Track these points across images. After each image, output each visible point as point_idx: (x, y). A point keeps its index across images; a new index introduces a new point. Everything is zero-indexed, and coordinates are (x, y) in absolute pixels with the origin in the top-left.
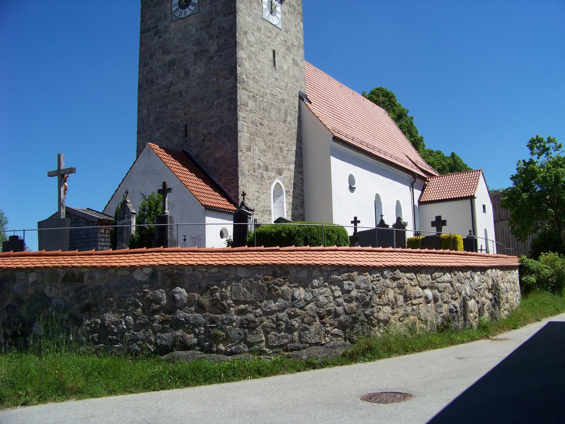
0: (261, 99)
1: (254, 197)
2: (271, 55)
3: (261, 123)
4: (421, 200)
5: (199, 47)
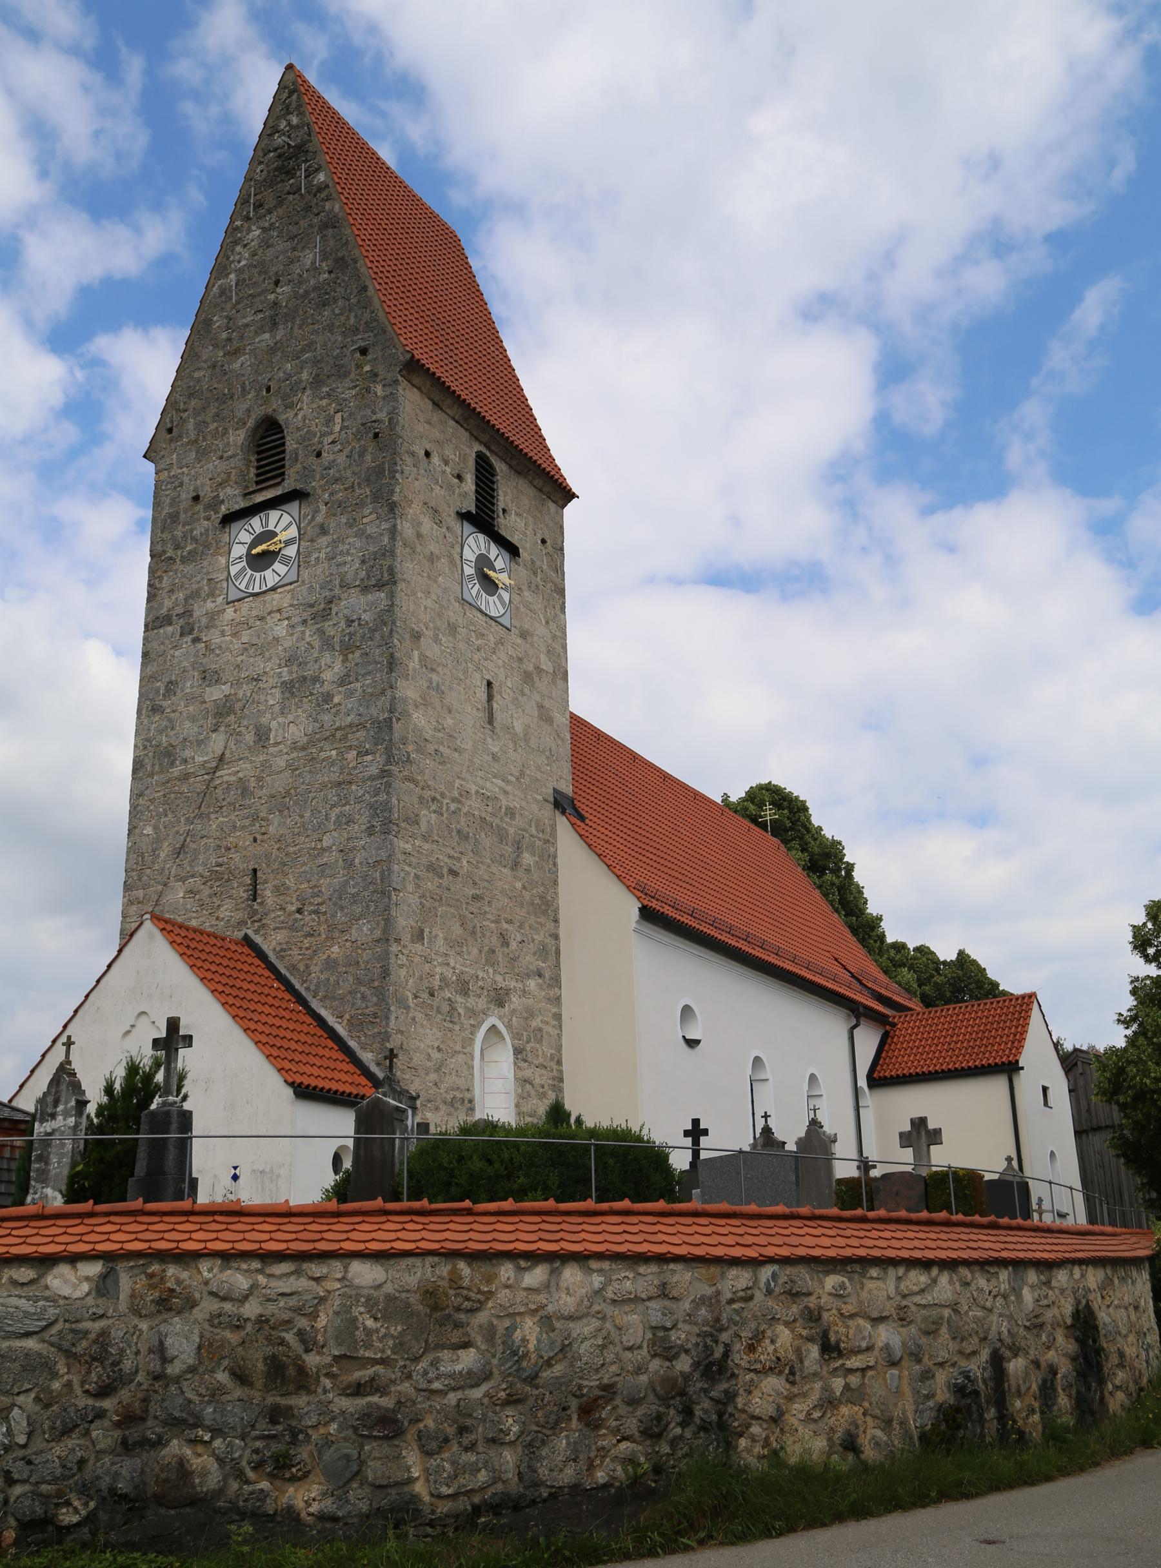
0: (453, 806)
1: (429, 1064)
2: (482, 694)
3: (453, 867)
4: (875, 1075)
5: (295, 668)
